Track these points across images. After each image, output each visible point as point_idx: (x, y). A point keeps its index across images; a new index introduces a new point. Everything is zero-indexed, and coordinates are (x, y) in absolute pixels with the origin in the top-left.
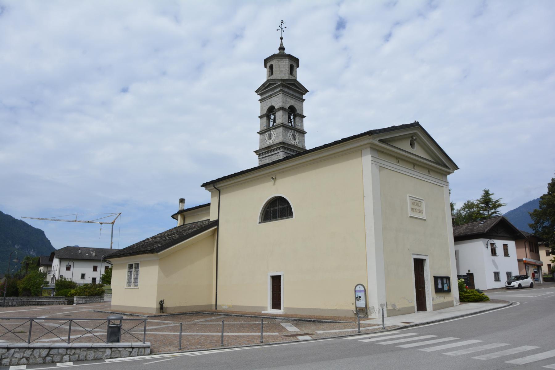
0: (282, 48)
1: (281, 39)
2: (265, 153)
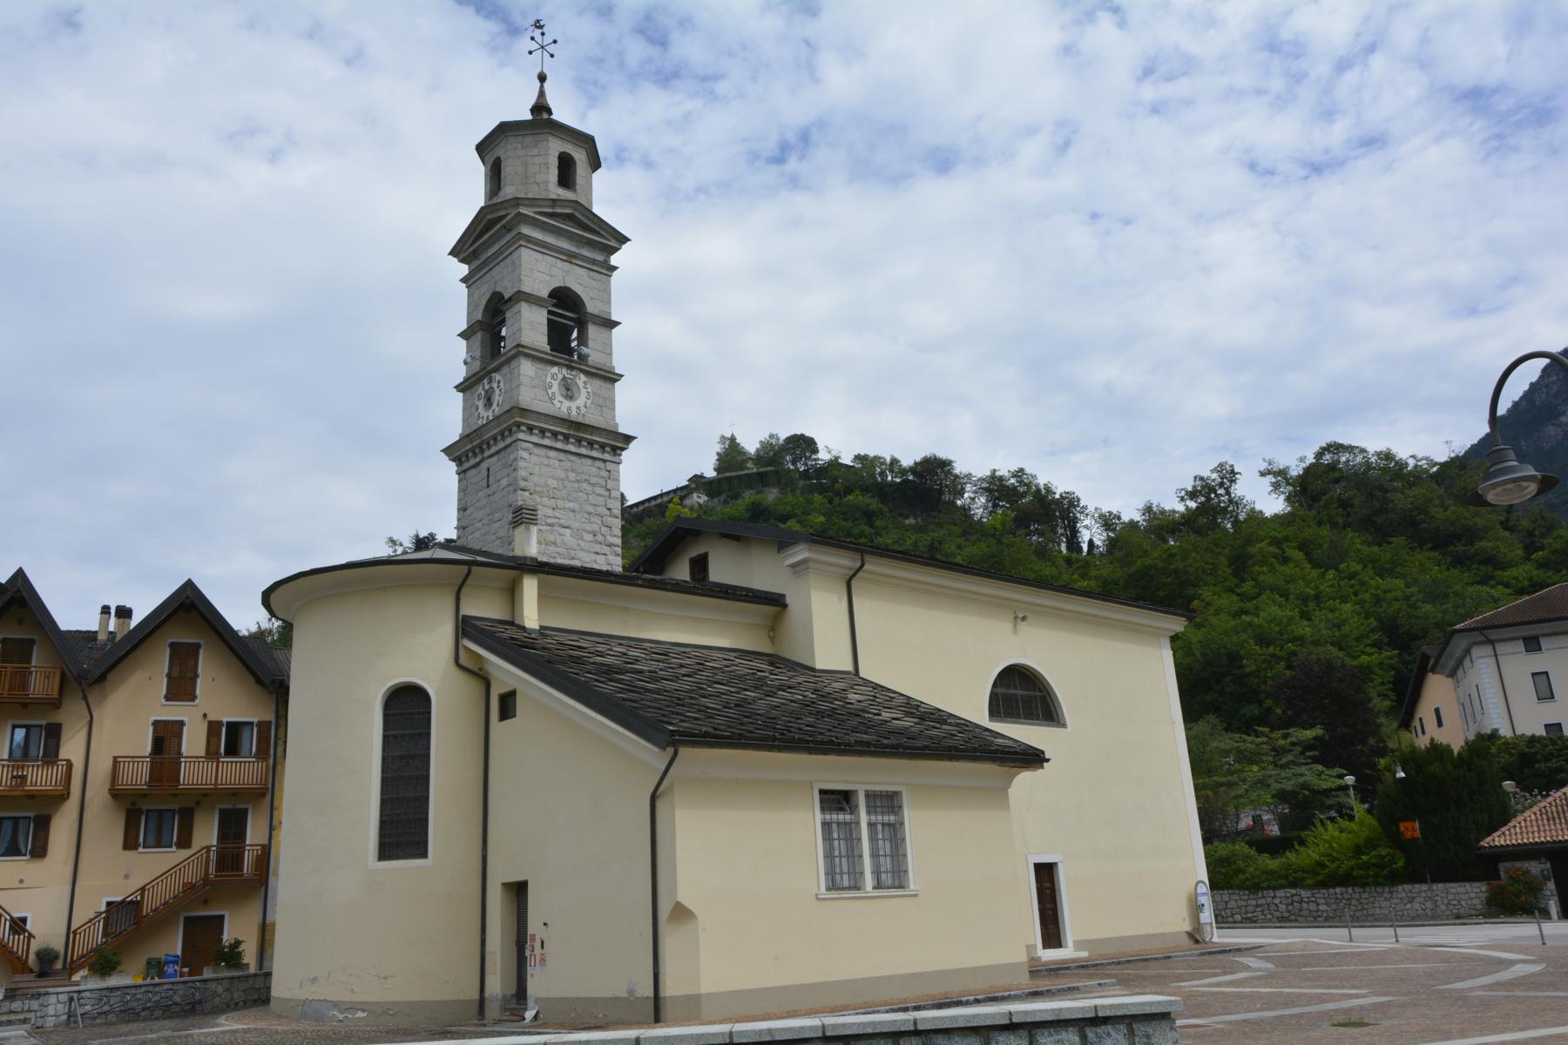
0: (541, 108)
1: (542, 78)
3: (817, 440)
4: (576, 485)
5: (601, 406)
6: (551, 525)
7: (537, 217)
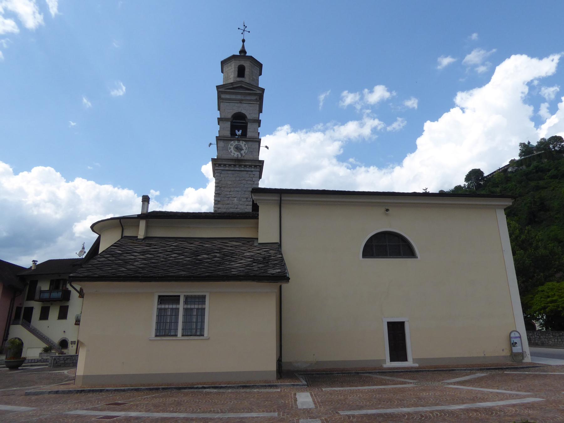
0: (243, 51)
1: (244, 41)
2: (230, 165)
3: (562, 137)
4: (239, 182)
5: (252, 152)
6: (229, 198)
7: (226, 90)
